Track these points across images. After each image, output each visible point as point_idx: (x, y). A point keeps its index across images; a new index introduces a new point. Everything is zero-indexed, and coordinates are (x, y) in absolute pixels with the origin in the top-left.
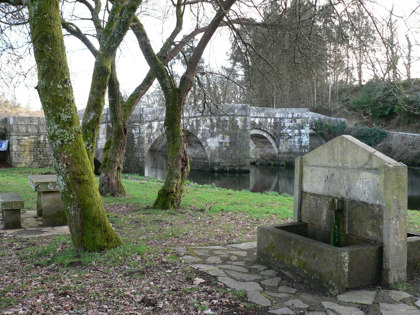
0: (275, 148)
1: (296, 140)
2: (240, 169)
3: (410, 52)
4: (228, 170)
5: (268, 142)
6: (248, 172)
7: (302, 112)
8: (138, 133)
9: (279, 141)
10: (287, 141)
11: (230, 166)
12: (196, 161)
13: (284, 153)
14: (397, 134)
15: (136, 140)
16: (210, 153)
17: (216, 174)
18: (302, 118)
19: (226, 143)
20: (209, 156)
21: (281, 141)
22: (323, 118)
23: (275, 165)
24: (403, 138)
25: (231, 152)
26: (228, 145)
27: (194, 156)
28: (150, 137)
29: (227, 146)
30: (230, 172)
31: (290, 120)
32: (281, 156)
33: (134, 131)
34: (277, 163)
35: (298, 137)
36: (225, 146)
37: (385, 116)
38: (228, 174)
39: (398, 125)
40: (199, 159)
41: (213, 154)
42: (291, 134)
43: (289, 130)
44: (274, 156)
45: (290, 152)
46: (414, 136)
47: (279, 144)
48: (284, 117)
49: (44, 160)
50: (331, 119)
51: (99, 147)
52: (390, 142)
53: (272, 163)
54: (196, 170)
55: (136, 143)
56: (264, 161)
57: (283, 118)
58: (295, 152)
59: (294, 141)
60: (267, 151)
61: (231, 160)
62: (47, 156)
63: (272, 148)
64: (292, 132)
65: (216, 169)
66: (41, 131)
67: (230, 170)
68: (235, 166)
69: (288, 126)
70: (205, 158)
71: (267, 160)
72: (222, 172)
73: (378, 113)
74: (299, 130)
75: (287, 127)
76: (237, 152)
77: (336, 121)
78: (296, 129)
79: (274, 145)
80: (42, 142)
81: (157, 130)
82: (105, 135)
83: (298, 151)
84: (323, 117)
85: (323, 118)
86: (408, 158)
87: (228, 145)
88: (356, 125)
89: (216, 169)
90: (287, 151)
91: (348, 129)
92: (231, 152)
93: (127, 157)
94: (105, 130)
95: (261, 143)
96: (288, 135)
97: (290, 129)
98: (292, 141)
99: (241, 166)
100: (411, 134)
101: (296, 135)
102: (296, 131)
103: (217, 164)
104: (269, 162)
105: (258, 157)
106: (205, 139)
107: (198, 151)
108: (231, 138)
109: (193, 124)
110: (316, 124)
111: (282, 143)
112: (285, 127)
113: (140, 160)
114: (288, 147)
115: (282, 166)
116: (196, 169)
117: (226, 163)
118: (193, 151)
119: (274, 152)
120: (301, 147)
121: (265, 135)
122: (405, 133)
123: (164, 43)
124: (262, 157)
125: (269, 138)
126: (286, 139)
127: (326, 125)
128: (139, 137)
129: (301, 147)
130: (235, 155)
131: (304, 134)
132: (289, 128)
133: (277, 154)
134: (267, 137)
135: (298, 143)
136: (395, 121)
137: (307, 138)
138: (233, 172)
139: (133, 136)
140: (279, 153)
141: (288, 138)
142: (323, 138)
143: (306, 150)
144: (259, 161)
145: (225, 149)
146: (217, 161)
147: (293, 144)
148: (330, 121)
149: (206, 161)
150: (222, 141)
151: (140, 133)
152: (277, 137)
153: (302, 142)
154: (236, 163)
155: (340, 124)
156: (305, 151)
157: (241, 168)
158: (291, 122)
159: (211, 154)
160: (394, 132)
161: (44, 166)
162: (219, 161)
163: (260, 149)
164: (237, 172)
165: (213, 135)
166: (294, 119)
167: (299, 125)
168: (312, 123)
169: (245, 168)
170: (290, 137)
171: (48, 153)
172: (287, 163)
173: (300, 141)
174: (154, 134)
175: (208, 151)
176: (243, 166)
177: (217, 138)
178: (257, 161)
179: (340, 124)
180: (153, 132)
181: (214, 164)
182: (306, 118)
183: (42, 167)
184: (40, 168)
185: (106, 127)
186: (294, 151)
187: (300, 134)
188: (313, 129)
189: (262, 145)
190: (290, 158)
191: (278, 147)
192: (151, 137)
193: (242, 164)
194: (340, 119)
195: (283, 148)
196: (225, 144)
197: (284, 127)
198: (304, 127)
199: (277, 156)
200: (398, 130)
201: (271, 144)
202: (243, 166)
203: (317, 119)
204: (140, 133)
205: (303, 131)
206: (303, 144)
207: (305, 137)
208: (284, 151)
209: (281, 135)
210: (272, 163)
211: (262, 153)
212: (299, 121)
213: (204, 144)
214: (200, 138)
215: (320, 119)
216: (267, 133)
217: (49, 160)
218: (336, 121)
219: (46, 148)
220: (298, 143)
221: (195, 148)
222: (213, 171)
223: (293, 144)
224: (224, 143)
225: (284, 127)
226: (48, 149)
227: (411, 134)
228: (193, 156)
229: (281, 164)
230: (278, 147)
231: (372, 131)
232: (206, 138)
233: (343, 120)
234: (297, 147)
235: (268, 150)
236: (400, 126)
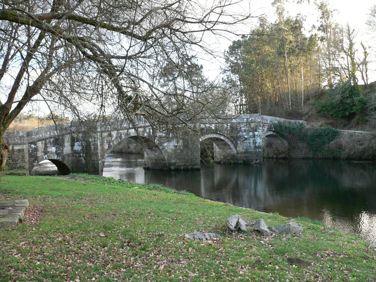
0: (234, 149)
1: (251, 141)
2: (192, 168)
3: (366, 57)
4: (182, 168)
5: (226, 144)
6: (200, 170)
7: (255, 117)
8: (94, 141)
9: (236, 142)
10: (243, 142)
11: (184, 165)
12: (158, 162)
13: (242, 153)
14: (347, 132)
15: (92, 146)
16: (167, 154)
17: (173, 173)
18: (255, 122)
19: (180, 146)
20: (166, 157)
21: (239, 142)
22: (282, 121)
23: (234, 163)
24: (351, 135)
25: (185, 152)
26: (182, 148)
27: (156, 158)
28: (110, 143)
29: (180, 149)
30: (184, 170)
31: (245, 124)
32: (239, 155)
33: (90, 140)
34: (236, 161)
35: (253, 139)
36: (179, 149)
37: (345, 116)
38: (182, 172)
39: (358, 124)
40: (160, 160)
41: (170, 156)
42: (246, 137)
43: (244, 133)
44: (233, 156)
45: (246, 152)
46: (362, 133)
47: (237, 145)
48: (240, 122)
49: (13, 164)
50: (291, 122)
51: (64, 153)
52: (342, 140)
53: (232, 162)
54: (158, 170)
55: (92, 149)
56: (227, 160)
57: (239, 123)
58: (251, 152)
59: (250, 142)
60: (228, 152)
61: (184, 161)
62: (15, 161)
63: (230, 148)
64: (248, 134)
65: (172, 168)
66: (10, 142)
67: (184, 169)
68: (188, 165)
69: (244, 130)
70: (163, 159)
71: (228, 160)
72: (178, 170)
73: (340, 114)
74: (253, 133)
75: (243, 130)
76: (190, 153)
77: (296, 123)
78: (250, 131)
79: (232, 146)
80: (11, 150)
81: (116, 138)
82: (70, 143)
83: (253, 151)
84: (282, 120)
85: (282, 121)
86: (355, 153)
87: (182, 148)
88: (321, 126)
89: (172, 168)
90: (244, 151)
91: (305, 130)
92: (185, 152)
93: (86, 160)
94: (70, 139)
95: (221, 145)
96: (244, 138)
97: (245, 132)
98: (248, 142)
99: (193, 165)
100: (359, 132)
101: (250, 137)
102: (251, 134)
103: (174, 164)
104: (230, 161)
105: (222, 157)
106: (161, 144)
107: (158, 154)
108: (184, 142)
109: (150, 132)
110: (275, 126)
111: (239, 145)
112: (241, 130)
113: (96, 162)
114: (245, 148)
115: (240, 164)
116: (158, 168)
117: (180, 163)
118: (155, 154)
119: (233, 152)
120: (256, 147)
121: (222, 138)
122: (354, 131)
123: (15, 78)
124: (225, 157)
125: (227, 140)
126: (242, 141)
127: (286, 127)
128: (94, 144)
129: (256, 147)
130: (188, 156)
131: (257, 136)
132: (245, 131)
133: (235, 154)
134: (225, 140)
135: (253, 144)
136: (354, 120)
137: (261, 139)
138: (186, 170)
139: (90, 143)
140: (237, 153)
141: (244, 140)
142: (283, 138)
143: (260, 150)
144: (222, 161)
145: (179, 151)
146: (173, 161)
147: (248, 145)
148: (290, 123)
149: (164, 162)
150: (176, 145)
151: (94, 141)
152: (234, 139)
153: (256, 143)
154: (188, 163)
155: (298, 125)
156: (259, 150)
157: (193, 167)
158: (246, 125)
159: (168, 156)
160: (345, 131)
161: (13, 168)
162: (175, 162)
163: (222, 150)
164: (189, 170)
165: (169, 140)
166: (248, 123)
167: (252, 128)
168: (271, 126)
169: (196, 167)
170: (246, 139)
171: (16, 159)
172: (244, 161)
173: (254, 142)
174: (113, 141)
175: (165, 154)
176: (195, 165)
177: (172, 142)
178: (221, 161)
179: (298, 125)
180: (113, 139)
181: (171, 164)
182: (259, 122)
183: (12, 169)
184: (9, 170)
185: (70, 137)
186: (249, 150)
187: (254, 136)
188: (272, 131)
189: (223, 147)
190: (246, 157)
191: (236, 148)
192: (111, 144)
193: (193, 163)
194: (298, 121)
195: (241, 148)
196: (179, 147)
197: (240, 131)
198: (257, 130)
199: (236, 156)
200: (358, 128)
201: (229, 145)
202: (195, 165)
203: (276, 122)
204: (94, 141)
205: (256, 133)
206: (257, 145)
207: (259, 138)
208: (242, 151)
209: (238, 138)
210: (232, 162)
211: (224, 154)
212: (253, 125)
213: (161, 148)
214: (157, 142)
215: (279, 122)
216: (225, 136)
217: (17, 164)
218: (296, 123)
219: (14, 155)
220: (253, 144)
221: (156, 151)
222: (170, 170)
223: (248, 145)
224: (178, 147)
225: (240, 131)
226: (16, 156)
227: (359, 132)
228: (156, 158)
229: (239, 163)
230: (236, 148)
231: (325, 130)
232: (163, 143)
233: (301, 121)
234: (252, 147)
235: (229, 151)
236: (359, 124)
